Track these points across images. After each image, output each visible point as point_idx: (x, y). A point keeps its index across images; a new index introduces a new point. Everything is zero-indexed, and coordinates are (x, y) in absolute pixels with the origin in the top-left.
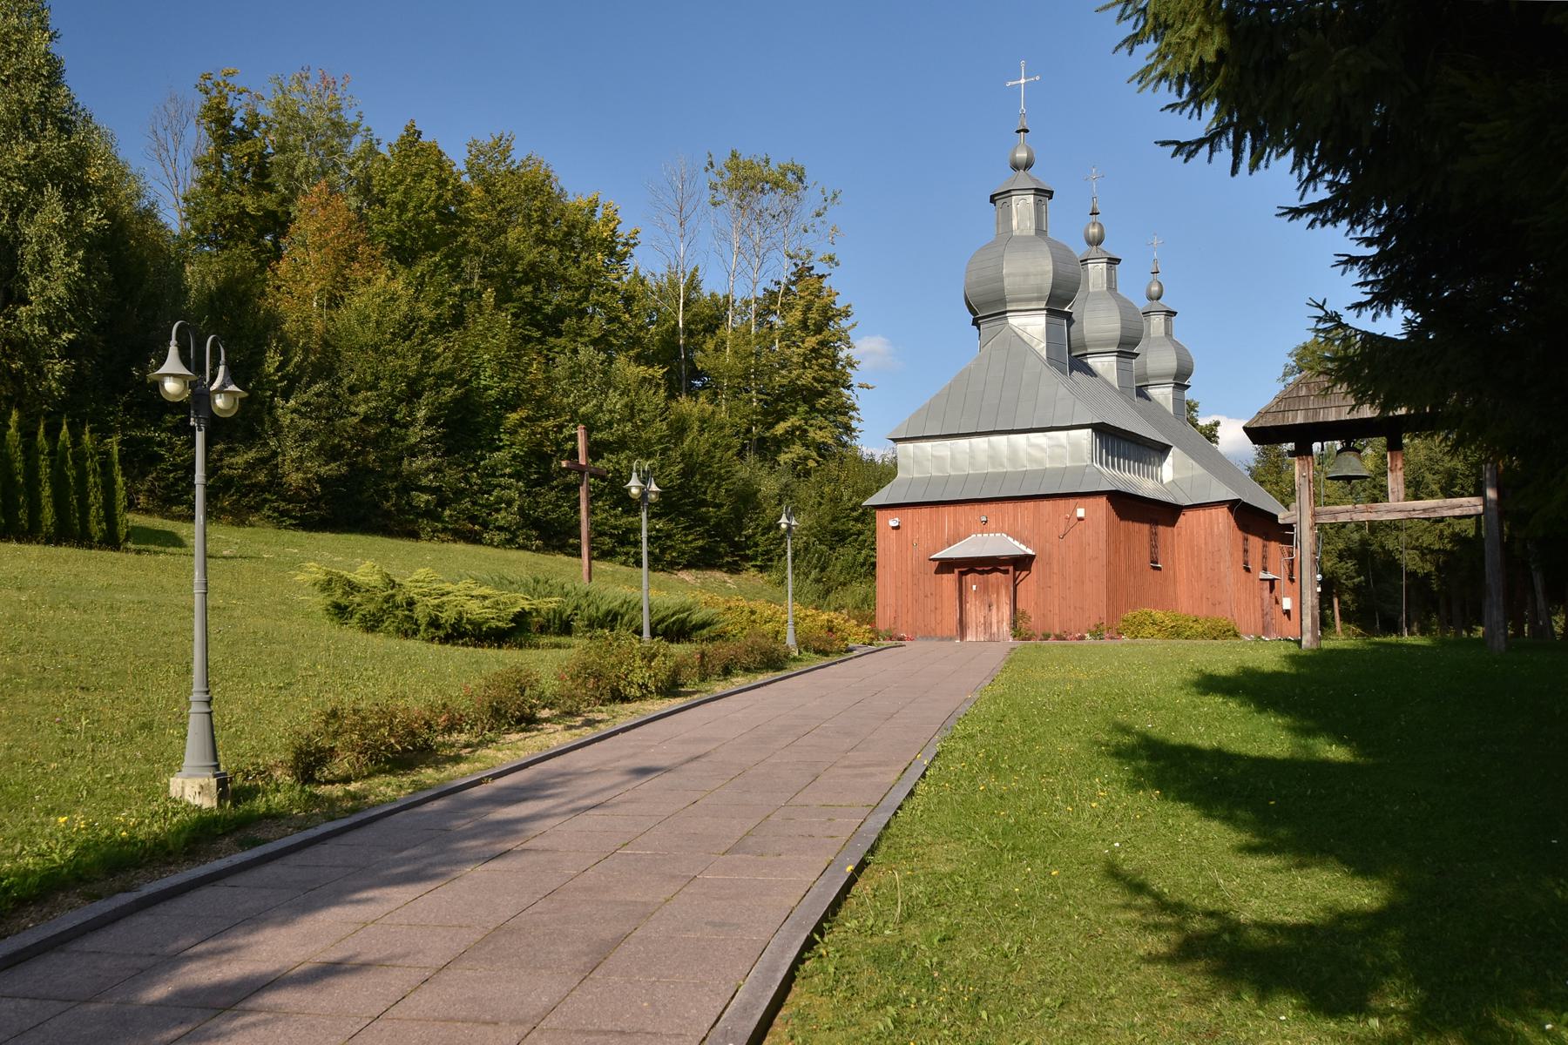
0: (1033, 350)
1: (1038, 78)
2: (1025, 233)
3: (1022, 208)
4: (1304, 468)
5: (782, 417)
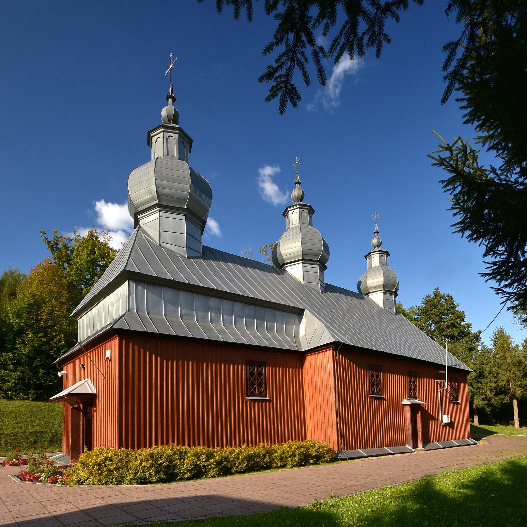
3: (376, 259)
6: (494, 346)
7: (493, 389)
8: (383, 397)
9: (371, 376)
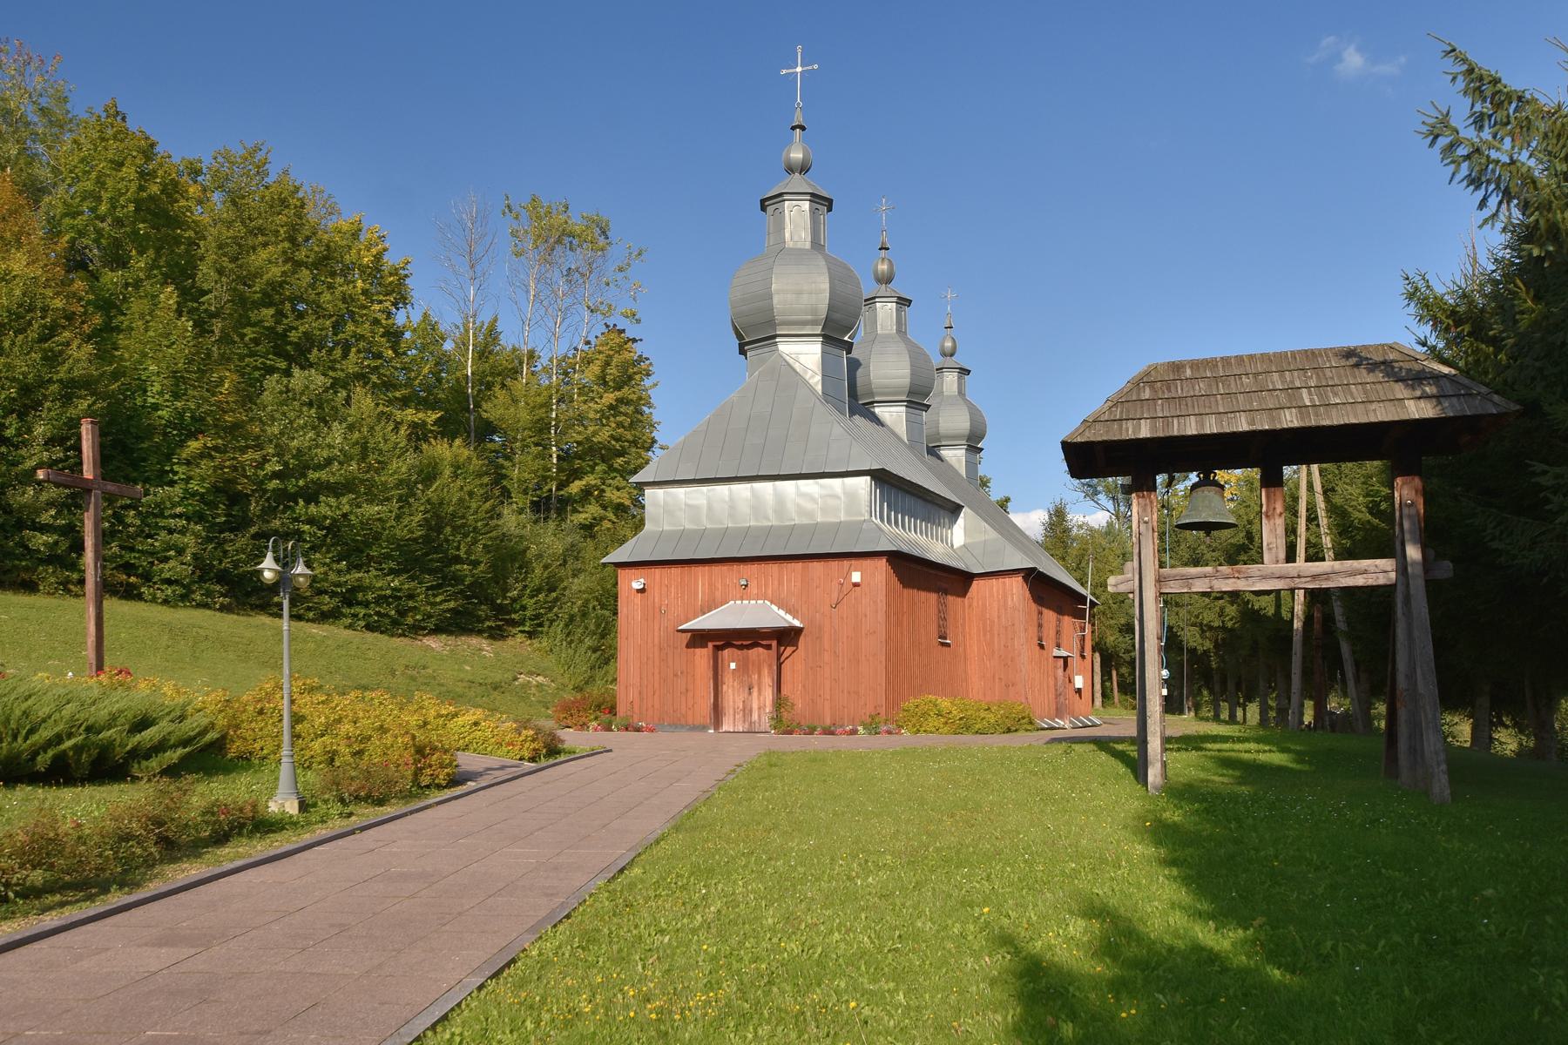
0: (806, 383)
1: (816, 66)
2: (799, 246)
3: (796, 216)
4: (1145, 510)
5: (576, 474)
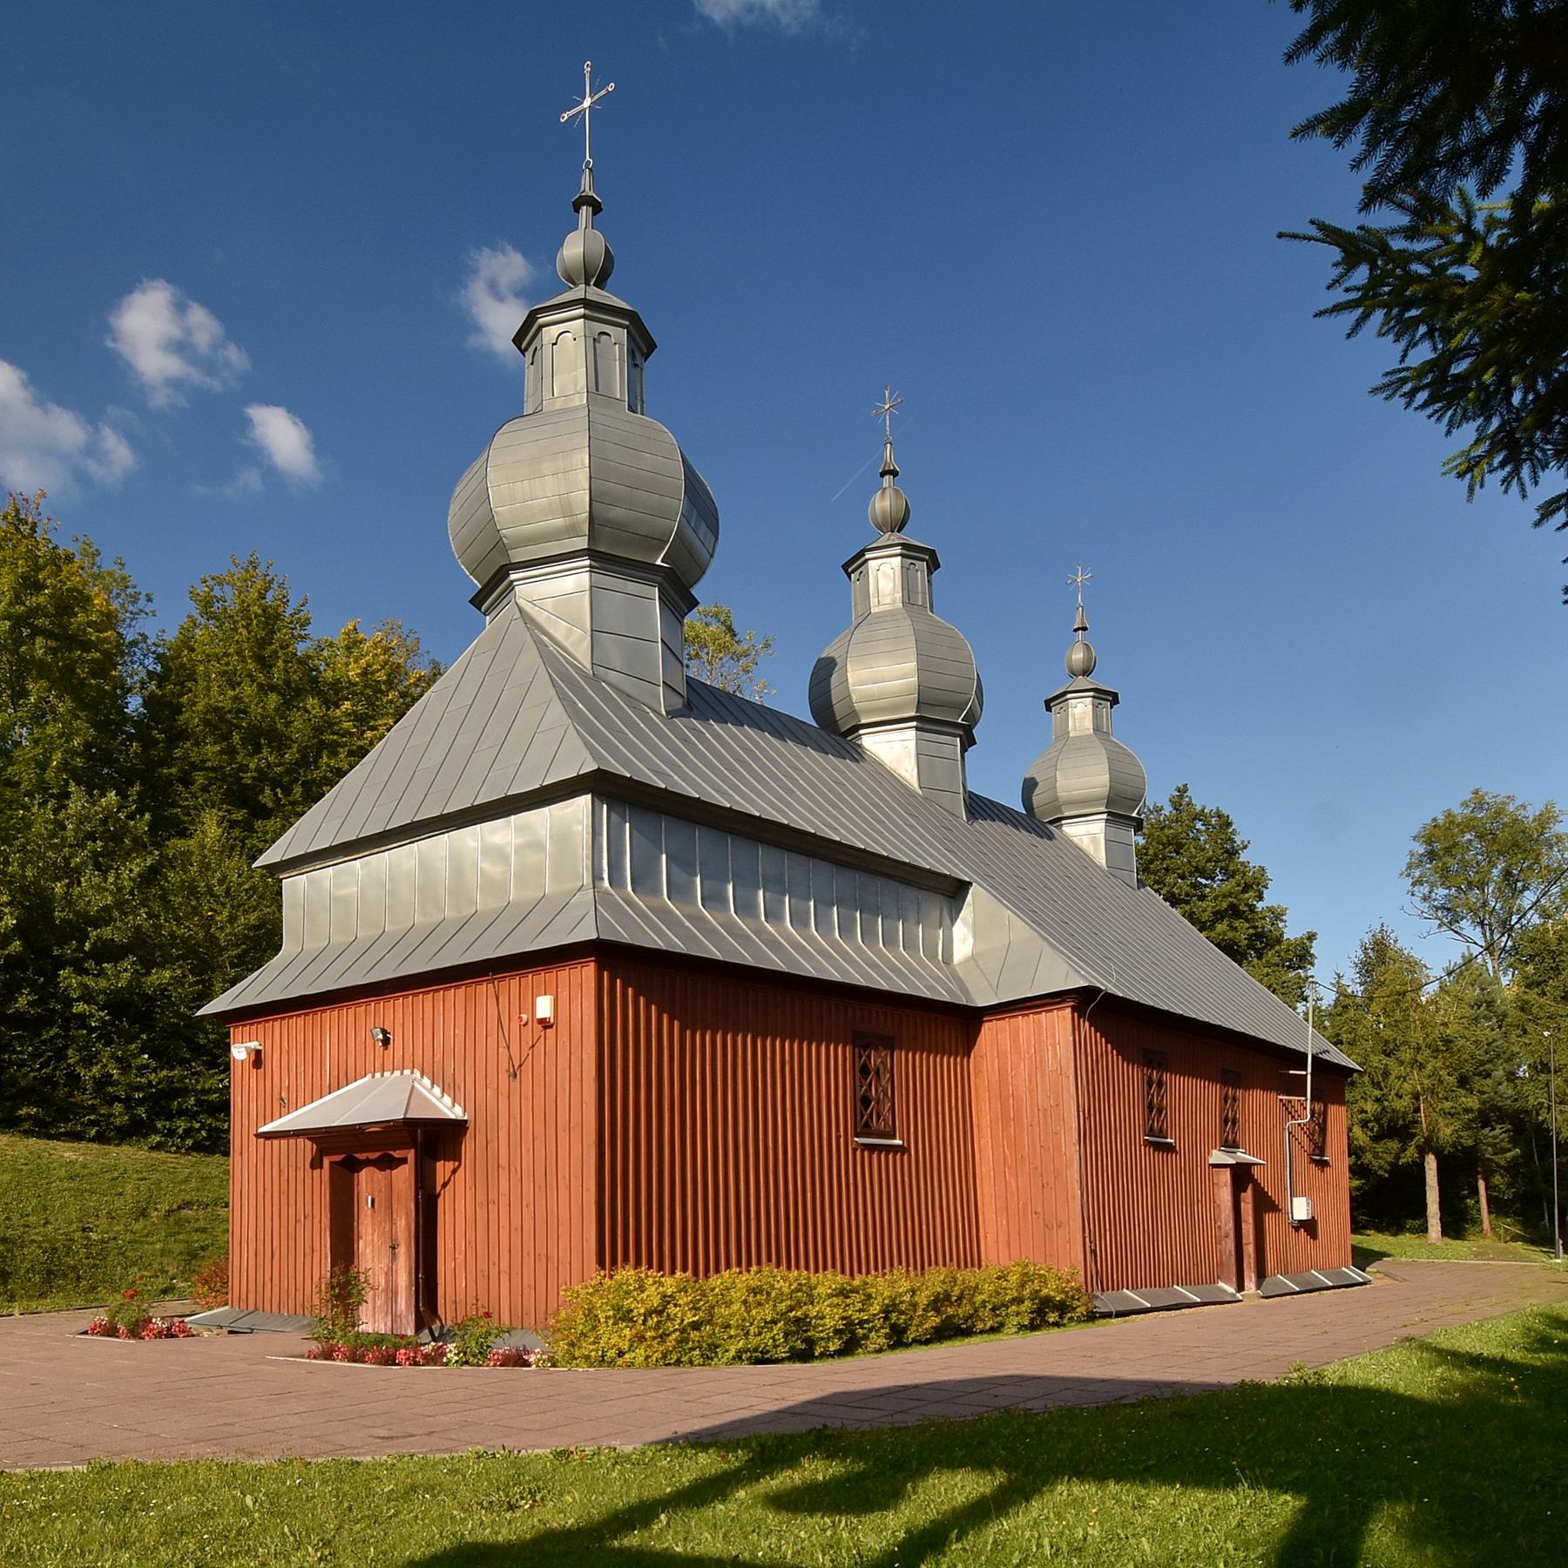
3: (1080, 711)
6: (1361, 984)
7: (1371, 1121)
8: (1171, 1144)
9: (1148, 1082)
